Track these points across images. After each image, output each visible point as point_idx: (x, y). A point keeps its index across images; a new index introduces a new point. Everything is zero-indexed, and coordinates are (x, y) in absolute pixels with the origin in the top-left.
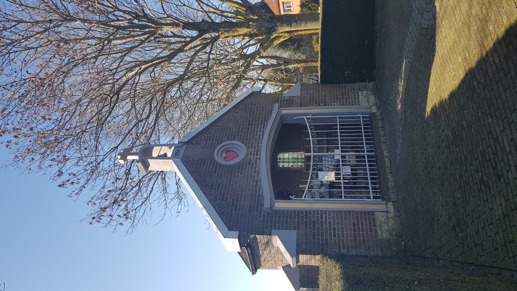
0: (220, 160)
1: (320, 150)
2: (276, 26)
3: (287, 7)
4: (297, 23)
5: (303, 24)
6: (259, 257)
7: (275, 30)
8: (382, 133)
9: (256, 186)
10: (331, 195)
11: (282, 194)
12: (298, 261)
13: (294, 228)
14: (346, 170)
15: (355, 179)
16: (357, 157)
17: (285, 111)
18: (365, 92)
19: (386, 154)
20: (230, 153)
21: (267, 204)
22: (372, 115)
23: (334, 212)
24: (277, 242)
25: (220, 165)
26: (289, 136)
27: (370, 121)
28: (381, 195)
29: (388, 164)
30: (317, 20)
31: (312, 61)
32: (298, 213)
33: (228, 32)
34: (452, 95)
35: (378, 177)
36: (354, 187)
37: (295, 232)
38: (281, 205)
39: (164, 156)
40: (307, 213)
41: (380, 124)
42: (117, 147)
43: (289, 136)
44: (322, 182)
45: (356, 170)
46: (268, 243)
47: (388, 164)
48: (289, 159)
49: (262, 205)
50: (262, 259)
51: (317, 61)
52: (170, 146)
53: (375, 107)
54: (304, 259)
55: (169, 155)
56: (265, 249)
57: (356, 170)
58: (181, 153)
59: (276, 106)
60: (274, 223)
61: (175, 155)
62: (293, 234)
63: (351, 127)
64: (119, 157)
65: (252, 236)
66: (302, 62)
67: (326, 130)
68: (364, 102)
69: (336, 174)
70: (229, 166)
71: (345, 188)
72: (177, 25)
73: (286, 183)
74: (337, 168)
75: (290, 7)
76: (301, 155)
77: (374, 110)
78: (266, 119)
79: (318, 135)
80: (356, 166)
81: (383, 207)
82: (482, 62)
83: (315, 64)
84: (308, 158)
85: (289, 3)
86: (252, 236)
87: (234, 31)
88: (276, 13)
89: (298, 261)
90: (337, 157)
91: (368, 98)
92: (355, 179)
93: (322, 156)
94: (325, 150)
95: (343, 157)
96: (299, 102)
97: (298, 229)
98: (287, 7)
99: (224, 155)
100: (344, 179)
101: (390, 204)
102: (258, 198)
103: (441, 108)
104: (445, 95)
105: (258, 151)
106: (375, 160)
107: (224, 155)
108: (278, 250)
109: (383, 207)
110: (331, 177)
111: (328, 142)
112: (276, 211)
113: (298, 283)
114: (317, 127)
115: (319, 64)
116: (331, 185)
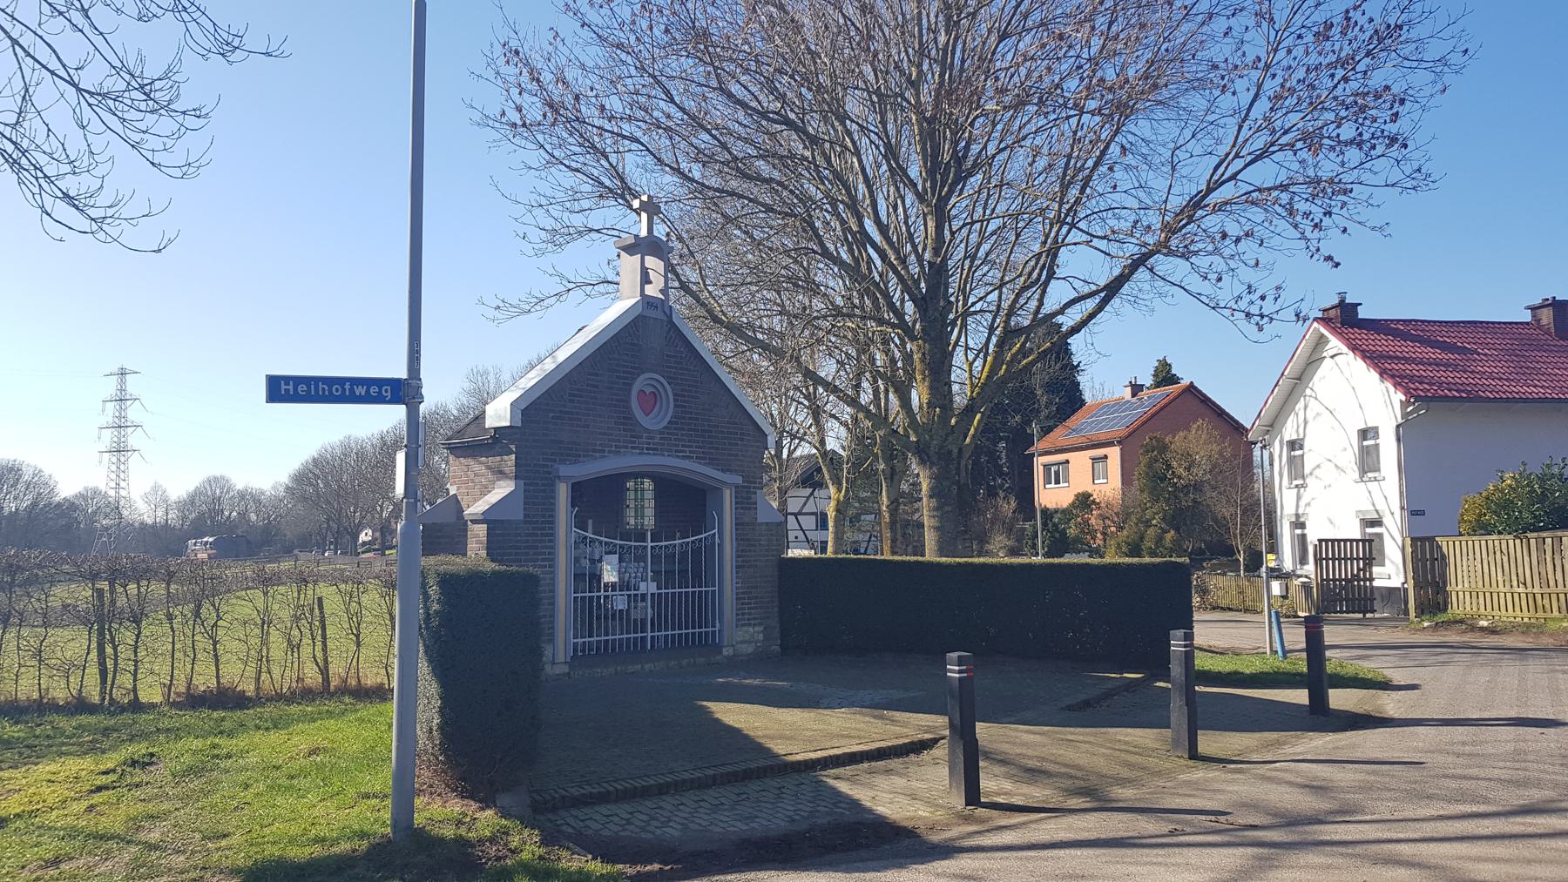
0: (640, 383)
1: (656, 558)
2: (932, 464)
3: (1057, 474)
4: (936, 509)
5: (934, 522)
6: (473, 456)
7: (922, 462)
8: (685, 662)
9: (594, 451)
10: (579, 577)
11: (579, 491)
12: (474, 522)
13: (526, 516)
14: (620, 603)
15: (606, 618)
16: (643, 621)
17: (727, 493)
18: (761, 637)
19: (647, 667)
20: (651, 400)
21: (564, 470)
22: (718, 648)
23: (553, 579)
24: (502, 490)
25: (631, 385)
26: (685, 503)
27: (709, 644)
28: (580, 657)
29: (631, 669)
30: (942, 551)
31: (894, 541)
32: (551, 521)
33: (922, 361)
34: (718, 721)
35: (606, 653)
36: (591, 613)
37: (521, 517)
38: (563, 492)
39: (645, 279)
40: (552, 536)
41: (701, 660)
42: (672, 101)
43: (685, 503)
44: (600, 560)
45: (621, 619)
46: (500, 474)
47: (631, 669)
48: (642, 509)
49: (563, 462)
50: (470, 461)
51: (894, 553)
52: (664, 291)
53: (731, 652)
54: (481, 530)
55: (651, 290)
56: (489, 468)
57: (621, 619)
58: (652, 313)
59: (739, 480)
60: (534, 486)
61: (647, 301)
62: (518, 514)
63: (702, 610)
64: (645, 198)
65: (513, 447)
66: (891, 515)
67: (697, 566)
68: (740, 634)
69: (614, 585)
70: (628, 401)
71: (591, 598)
72: (936, 251)
73: (600, 501)
74: (623, 585)
75: (1058, 482)
76: (649, 521)
77: (725, 652)
78: (712, 462)
79: (684, 554)
80: (628, 619)
81: (561, 657)
82: (746, 737)
83: (886, 548)
84: (641, 536)
85: (1067, 481)
86: (513, 447)
87: (923, 373)
88: (1040, 445)
89: (474, 522)
90: (643, 586)
91: (749, 642)
92: (606, 618)
93: (645, 562)
94: (656, 568)
95: (644, 596)
96: (746, 520)
97: (525, 522)
98: (1057, 474)
99: (648, 390)
100: (606, 597)
101: (566, 669)
102: (573, 454)
103: (708, 713)
104: (717, 716)
105: (654, 450)
106: (637, 650)
107: (648, 390)
108: (486, 490)
109: (561, 657)
110: (610, 575)
111: (670, 573)
112: (553, 485)
113: (429, 521)
114: (696, 552)
115: (888, 556)
116: (596, 577)
